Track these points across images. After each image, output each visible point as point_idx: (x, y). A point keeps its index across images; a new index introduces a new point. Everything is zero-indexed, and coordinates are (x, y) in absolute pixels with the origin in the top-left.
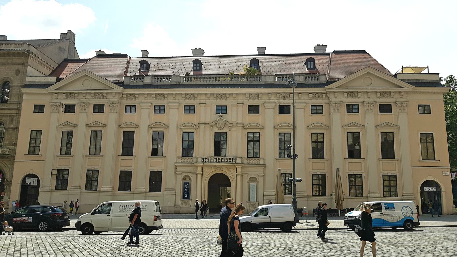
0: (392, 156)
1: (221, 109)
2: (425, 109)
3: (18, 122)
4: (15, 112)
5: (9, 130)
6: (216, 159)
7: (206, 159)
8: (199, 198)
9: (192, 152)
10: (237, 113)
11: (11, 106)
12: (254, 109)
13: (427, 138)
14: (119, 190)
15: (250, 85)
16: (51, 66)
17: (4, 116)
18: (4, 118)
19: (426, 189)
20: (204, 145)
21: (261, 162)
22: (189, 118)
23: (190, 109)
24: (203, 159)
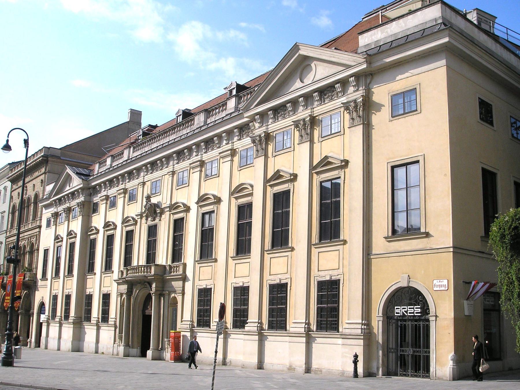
19: (399, 310)
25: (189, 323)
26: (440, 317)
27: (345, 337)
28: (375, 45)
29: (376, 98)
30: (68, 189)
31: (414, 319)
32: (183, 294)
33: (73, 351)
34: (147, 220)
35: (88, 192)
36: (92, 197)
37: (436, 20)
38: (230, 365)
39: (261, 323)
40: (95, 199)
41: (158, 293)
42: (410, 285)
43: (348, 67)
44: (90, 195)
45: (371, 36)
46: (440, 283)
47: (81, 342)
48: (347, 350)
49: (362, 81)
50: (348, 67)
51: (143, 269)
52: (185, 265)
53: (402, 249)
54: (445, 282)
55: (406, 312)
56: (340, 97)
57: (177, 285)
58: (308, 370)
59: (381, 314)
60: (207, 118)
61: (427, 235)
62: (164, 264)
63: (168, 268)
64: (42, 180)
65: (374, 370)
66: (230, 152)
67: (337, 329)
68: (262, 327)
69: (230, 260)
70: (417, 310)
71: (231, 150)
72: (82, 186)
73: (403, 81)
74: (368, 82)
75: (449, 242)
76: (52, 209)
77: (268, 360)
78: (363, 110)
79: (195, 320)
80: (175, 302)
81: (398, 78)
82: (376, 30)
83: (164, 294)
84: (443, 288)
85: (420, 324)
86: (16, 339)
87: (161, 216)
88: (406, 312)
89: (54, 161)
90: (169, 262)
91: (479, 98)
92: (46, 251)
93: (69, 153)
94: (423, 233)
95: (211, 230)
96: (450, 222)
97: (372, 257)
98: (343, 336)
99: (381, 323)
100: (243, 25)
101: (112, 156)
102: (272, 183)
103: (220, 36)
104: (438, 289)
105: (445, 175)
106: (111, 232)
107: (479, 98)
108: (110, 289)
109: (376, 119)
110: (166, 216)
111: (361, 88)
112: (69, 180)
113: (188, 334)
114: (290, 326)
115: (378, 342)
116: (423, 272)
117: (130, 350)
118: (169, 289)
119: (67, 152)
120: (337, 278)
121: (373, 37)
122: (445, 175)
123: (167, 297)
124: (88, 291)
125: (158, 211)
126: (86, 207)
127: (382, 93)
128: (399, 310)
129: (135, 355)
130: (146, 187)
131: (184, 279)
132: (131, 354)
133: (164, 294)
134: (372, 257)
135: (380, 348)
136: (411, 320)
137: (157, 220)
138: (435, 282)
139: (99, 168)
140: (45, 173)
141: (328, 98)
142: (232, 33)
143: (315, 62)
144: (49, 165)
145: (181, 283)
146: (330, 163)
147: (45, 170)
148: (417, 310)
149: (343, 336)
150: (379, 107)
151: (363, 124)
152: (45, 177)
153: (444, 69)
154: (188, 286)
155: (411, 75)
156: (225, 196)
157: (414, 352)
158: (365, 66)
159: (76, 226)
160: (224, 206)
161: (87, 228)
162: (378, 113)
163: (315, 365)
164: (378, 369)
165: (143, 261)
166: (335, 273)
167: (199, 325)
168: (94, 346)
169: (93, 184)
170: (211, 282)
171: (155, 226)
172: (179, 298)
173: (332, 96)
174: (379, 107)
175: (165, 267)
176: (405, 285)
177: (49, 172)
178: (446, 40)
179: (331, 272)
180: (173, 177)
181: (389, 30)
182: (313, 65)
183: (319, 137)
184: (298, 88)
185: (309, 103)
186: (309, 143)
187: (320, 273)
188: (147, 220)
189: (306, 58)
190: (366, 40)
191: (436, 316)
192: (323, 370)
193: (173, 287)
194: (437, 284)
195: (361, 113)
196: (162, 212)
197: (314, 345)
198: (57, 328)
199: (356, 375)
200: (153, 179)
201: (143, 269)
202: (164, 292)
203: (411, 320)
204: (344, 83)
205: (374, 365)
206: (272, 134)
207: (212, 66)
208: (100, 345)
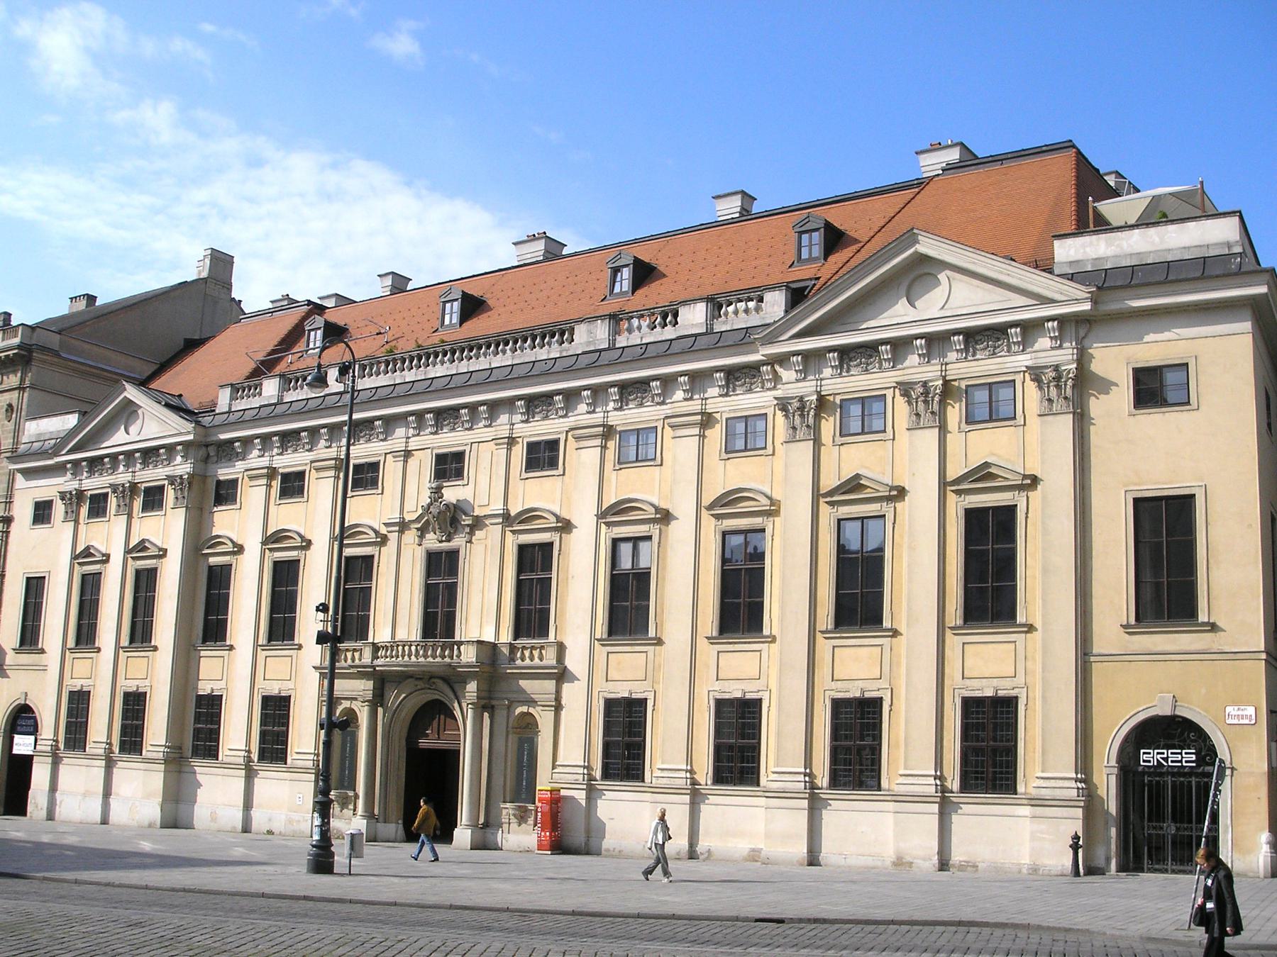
19: (1150, 757)
20: (395, 614)
25: (312, 757)
26: (1240, 770)
27: (898, 798)
28: (1093, 265)
29: (1096, 367)
30: (119, 440)
31: (1180, 772)
32: (558, 708)
33: (164, 826)
34: (422, 537)
35: (202, 452)
36: (211, 467)
37: (1229, 245)
38: (707, 858)
39: (110, 744)
40: (220, 471)
41: (483, 702)
42: (1178, 713)
43: (1045, 301)
44: (206, 459)
45: (1083, 246)
46: (1240, 713)
47: (182, 807)
48: (1043, 827)
49: (1070, 330)
50: (1045, 301)
51: (413, 648)
52: (561, 648)
53: (1159, 649)
54: (1250, 711)
55: (1166, 759)
56: (1016, 353)
57: (540, 689)
58: (944, 865)
59: (1113, 762)
60: (616, 332)
61: (1213, 627)
62: (489, 637)
63: (506, 651)
64: (10, 406)
65: (1100, 862)
66: (699, 417)
67: (640, 777)
68: (812, 782)
69: (702, 644)
70: (1187, 757)
71: (702, 414)
72: (191, 437)
73: (1157, 347)
74: (1082, 333)
75: (1257, 640)
76: (60, 480)
77: (829, 848)
78: (1074, 386)
79: (61, 738)
80: (528, 727)
81: (1147, 338)
82: (1094, 237)
83: (493, 707)
84: (1247, 722)
85: (1190, 782)
86: (16, 803)
87: (472, 533)
88: (1166, 759)
89: (44, 362)
90: (506, 637)
91: (664, 276)
92: (35, 586)
93: (77, 343)
94: (1204, 624)
95: (642, 579)
96: (1258, 609)
97: (1092, 659)
98: (1033, 802)
99: (1113, 779)
100: (208, 28)
101: (282, 376)
102: (835, 499)
103: (149, 47)
104: (1236, 721)
105: (1250, 526)
106: (292, 554)
107: (664, 276)
108: (290, 685)
109: (1097, 406)
110: (490, 536)
111: (1066, 345)
112: (125, 415)
113: (581, 796)
114: (224, 753)
115: (1107, 812)
116: (1203, 691)
117: (380, 826)
118: (509, 696)
119: (73, 341)
120: (1013, 693)
121: (1088, 250)
122: (1250, 526)
123: (501, 715)
124: (205, 688)
125: (467, 521)
126: (195, 487)
127: (1115, 360)
128: (1150, 757)
129: (392, 836)
130: (412, 462)
131: (562, 675)
132: (380, 835)
133: (493, 707)
134: (1092, 659)
135: (1112, 822)
136: (1173, 775)
137: (458, 541)
138: (1229, 709)
139: (232, 399)
140: (21, 388)
141: (985, 349)
142: (178, 45)
143: (948, 272)
144: (34, 369)
145: (550, 685)
146: (991, 476)
147: (22, 380)
148: (1187, 757)
149: (1033, 802)
150: (1105, 386)
151: (1074, 413)
152: (20, 399)
153: (1248, 339)
154: (573, 694)
155: (1177, 337)
156: (684, 509)
157: (1178, 829)
158: (1087, 306)
159: (167, 529)
160: (681, 533)
161: (199, 540)
162: (1102, 397)
163: (957, 856)
164: (1108, 860)
165: (410, 628)
166: (1007, 683)
167: (262, 757)
168: (239, 815)
169: (223, 436)
170: (645, 686)
171: (453, 555)
172: (544, 719)
173: (995, 348)
174: (1105, 386)
175: (494, 647)
176: (1166, 711)
177: (32, 387)
178: (1263, 289)
179: (995, 682)
180: (509, 449)
181: (1125, 244)
182: (942, 277)
183: (960, 422)
184: (898, 317)
185: (935, 351)
186: (937, 430)
187: (968, 682)
188: (422, 537)
189: (923, 259)
190: (1072, 252)
191: (1233, 769)
192: (980, 865)
193: (523, 691)
194: (1233, 713)
195: (1069, 392)
196: (478, 523)
197: (954, 817)
198: (101, 773)
199: (1077, 874)
200: (439, 447)
201: (413, 648)
202: (494, 702)
203: (1173, 775)
204: (1030, 329)
205: (1100, 853)
206: (831, 398)
207: (121, 117)
208: (256, 814)
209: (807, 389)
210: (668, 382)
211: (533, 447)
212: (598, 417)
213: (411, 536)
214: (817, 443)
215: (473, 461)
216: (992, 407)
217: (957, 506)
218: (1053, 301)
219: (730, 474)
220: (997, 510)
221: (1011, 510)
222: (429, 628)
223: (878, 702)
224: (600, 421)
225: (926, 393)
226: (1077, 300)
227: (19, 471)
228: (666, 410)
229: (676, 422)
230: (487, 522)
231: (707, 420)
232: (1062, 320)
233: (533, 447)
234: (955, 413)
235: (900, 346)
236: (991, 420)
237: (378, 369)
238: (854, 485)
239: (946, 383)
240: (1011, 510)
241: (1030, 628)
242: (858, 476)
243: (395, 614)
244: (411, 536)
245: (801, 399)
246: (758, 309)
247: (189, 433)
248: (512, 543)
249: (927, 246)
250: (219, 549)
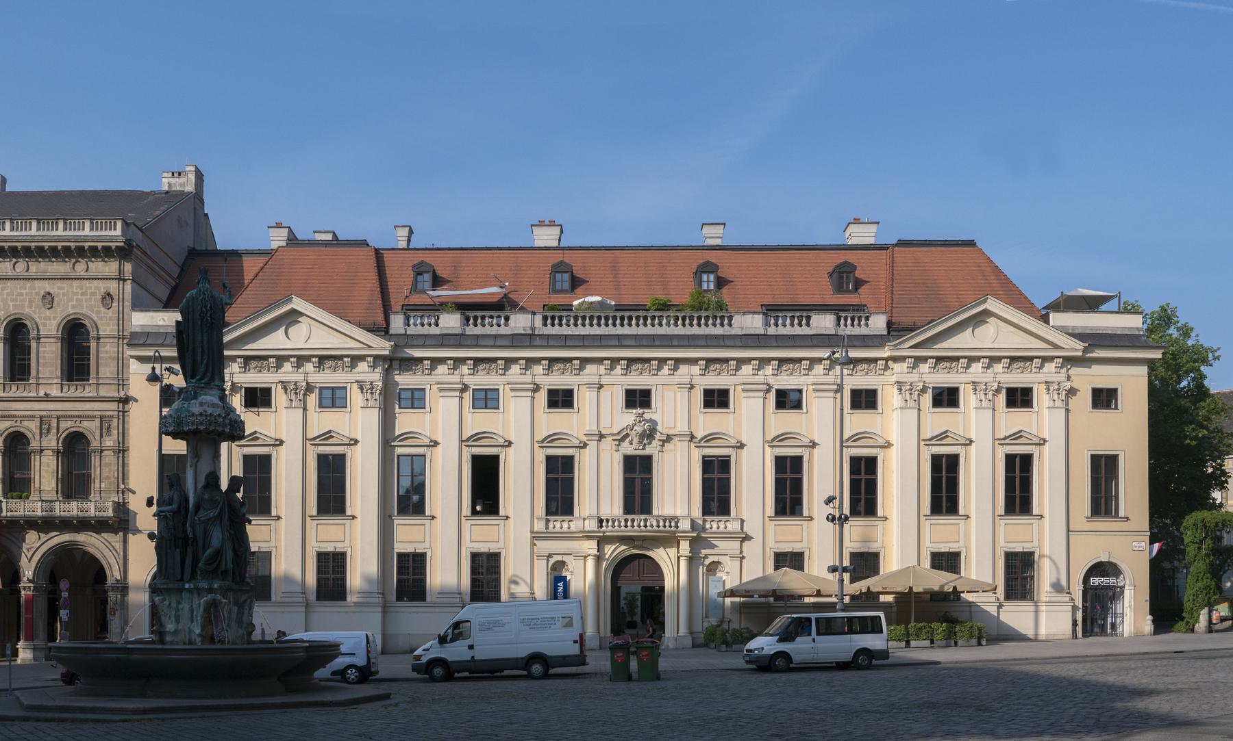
0: (952, 509)
1: (638, 399)
2: (1104, 398)
3: (124, 434)
4: (114, 406)
5: (105, 453)
6: (626, 521)
7: (608, 521)
8: (590, 631)
9: (1156, 546)
10: (675, 406)
11: (103, 392)
12: (717, 399)
13: (1104, 468)
14: (704, 457)
15: (706, 337)
16: (163, 269)
17: (84, 417)
18: (86, 424)
19: (1096, 581)
20: (599, 490)
21: (733, 526)
22: (559, 421)
23: (561, 399)
24: (601, 521)
27: (280, 604)
43: (1057, 347)
128: (1096, 581)
146: (257, 438)
184: (276, 341)
204: (355, 359)
209: (298, 377)
210: (510, 361)
211: (856, 394)
212: (760, 378)
213: (608, 443)
214: (305, 409)
215: (659, 398)
216: (334, 398)
217: (467, 454)
218: (370, 347)
219: (478, 421)
220: (563, 457)
221: (572, 458)
222: (628, 509)
223: (422, 557)
224: (530, 381)
225: (296, 389)
226: (1075, 347)
227: (132, 357)
228: (810, 379)
229: (749, 389)
230: (676, 439)
231: (465, 388)
232: (376, 357)
233: (856, 394)
234: (313, 399)
235: (281, 360)
236: (333, 406)
237: (568, 321)
238: (328, 435)
239: (308, 384)
240: (572, 458)
241: (354, 517)
242: (330, 431)
243: (599, 490)
244: (608, 443)
245: (295, 384)
246: (506, 324)
247: (384, 348)
248: (697, 456)
249: (298, 304)
250: (1022, 440)
